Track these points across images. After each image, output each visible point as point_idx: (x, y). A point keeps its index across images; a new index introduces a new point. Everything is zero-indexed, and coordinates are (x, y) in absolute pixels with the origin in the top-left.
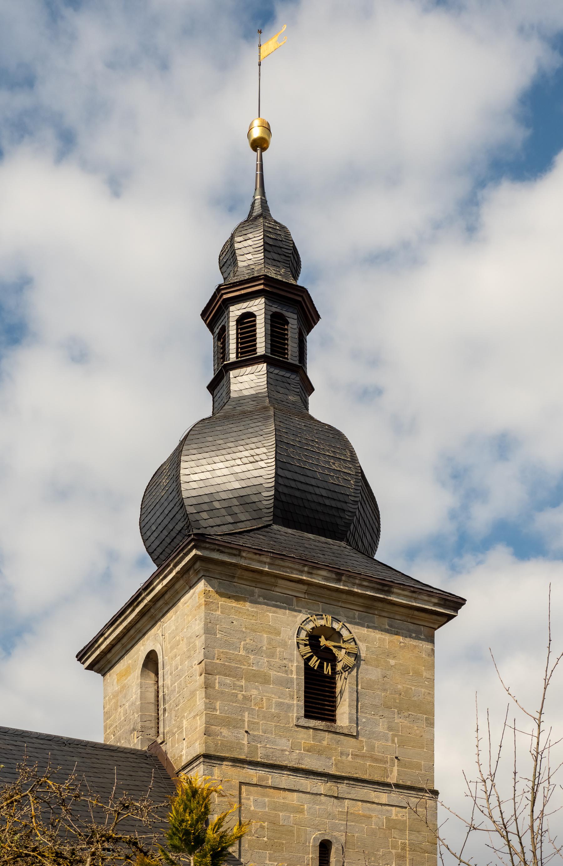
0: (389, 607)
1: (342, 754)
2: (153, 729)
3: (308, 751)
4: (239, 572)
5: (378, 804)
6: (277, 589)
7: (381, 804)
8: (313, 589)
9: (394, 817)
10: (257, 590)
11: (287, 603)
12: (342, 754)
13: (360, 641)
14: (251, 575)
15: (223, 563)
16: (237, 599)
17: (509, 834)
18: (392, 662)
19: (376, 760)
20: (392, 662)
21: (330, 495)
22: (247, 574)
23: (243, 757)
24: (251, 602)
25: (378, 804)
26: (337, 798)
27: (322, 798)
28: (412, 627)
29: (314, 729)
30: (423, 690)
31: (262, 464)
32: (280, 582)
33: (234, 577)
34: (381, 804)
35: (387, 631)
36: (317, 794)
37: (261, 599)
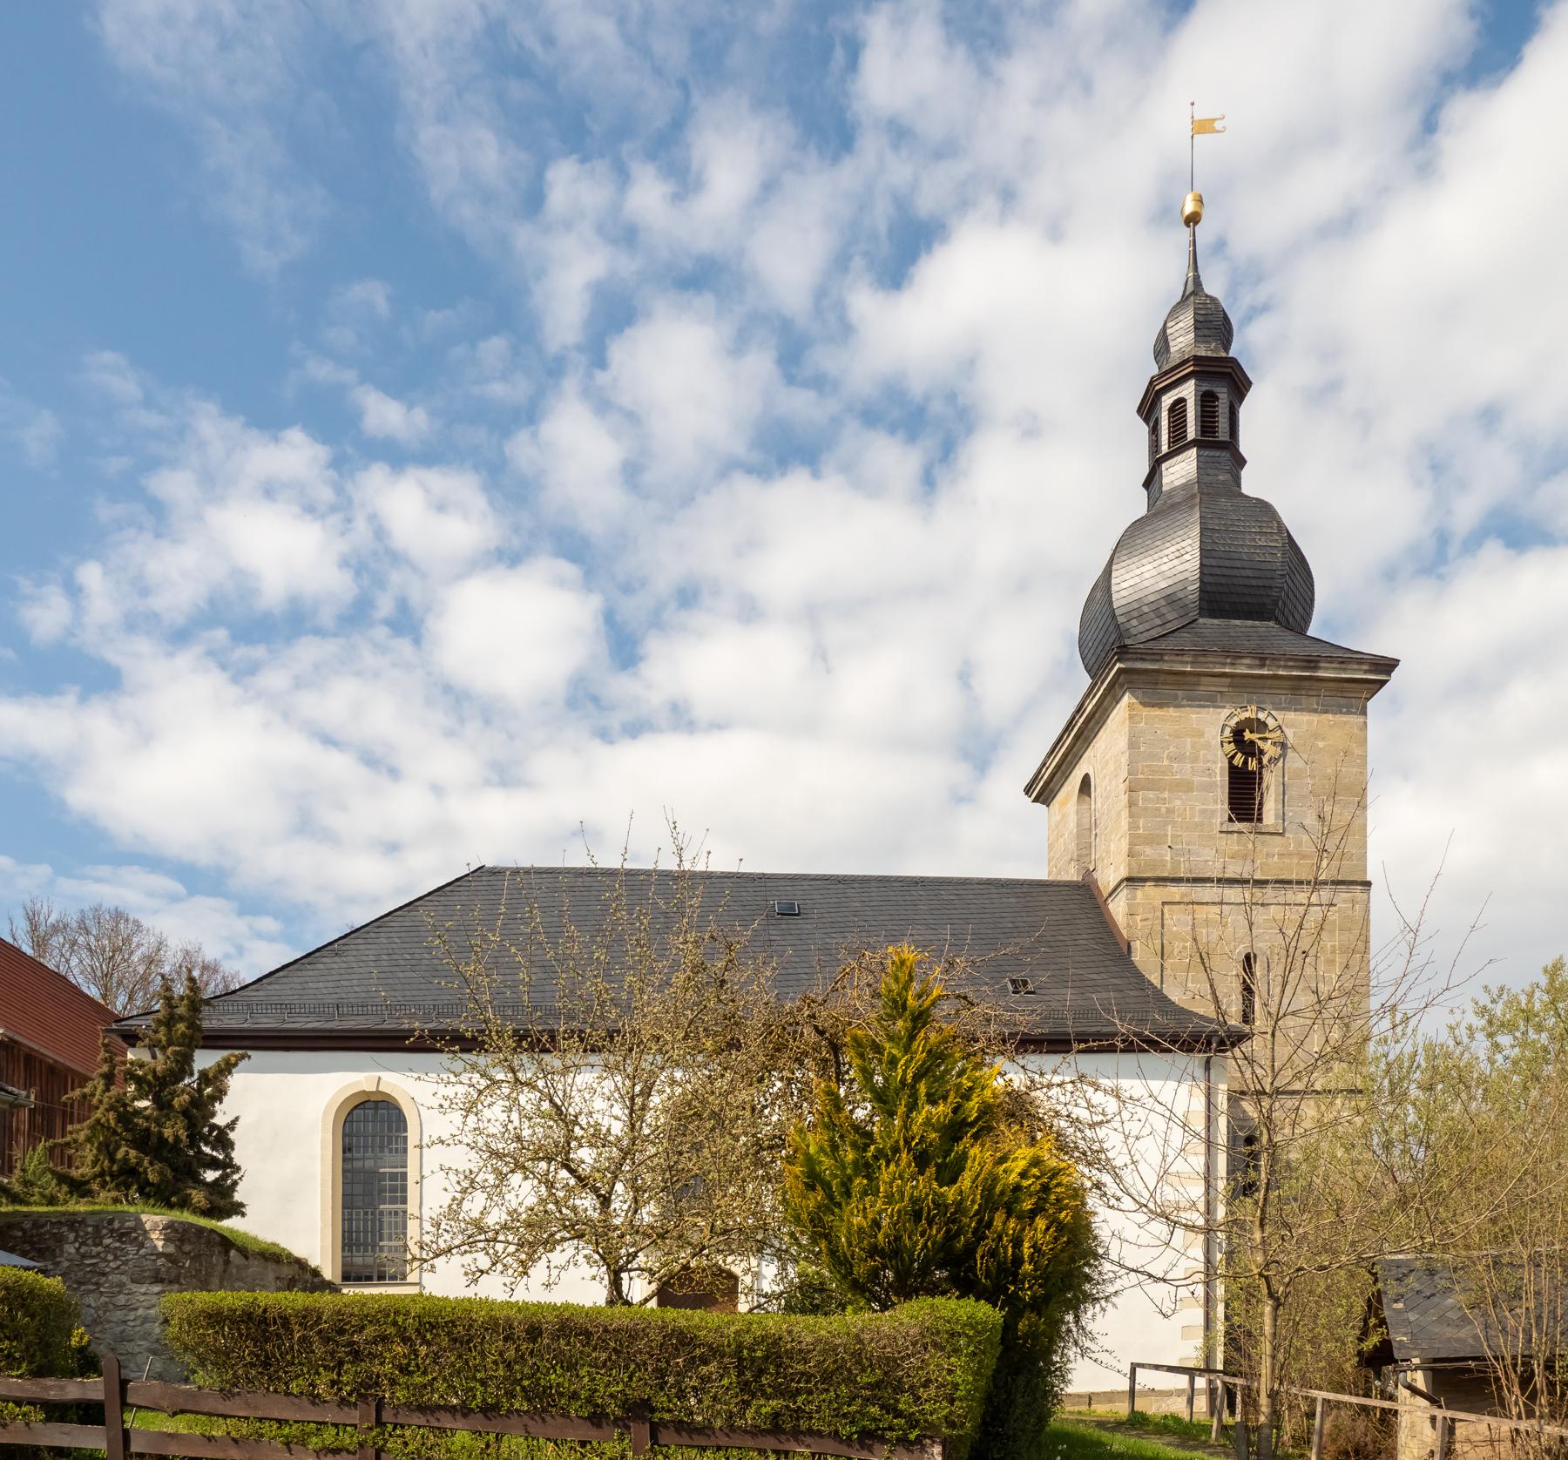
0: (1316, 684)
8: (1236, 681)
11: (1211, 701)
18: (1321, 744)
20: (1321, 744)
21: (1256, 574)
23: (1166, 875)
28: (1342, 701)
31: (1187, 557)
32: (1204, 679)
35: (1315, 711)
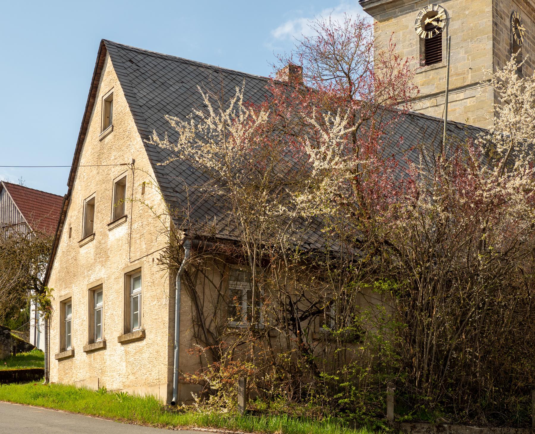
1: (440, 79)
2: (443, 106)
3: (423, 85)
4: (385, 6)
5: (459, 100)
6: (406, 4)
7: (461, 100)
9: (469, 105)
10: (397, 10)
12: (440, 79)
13: (449, 9)
14: (391, 5)
15: (377, 6)
16: (388, 20)
17: (450, 88)
18: (467, 12)
19: (459, 75)
20: (467, 12)
22: (389, 6)
24: (395, 18)
25: (459, 100)
26: (437, 106)
27: (430, 109)
29: (425, 72)
30: (485, 20)
33: (385, 10)
34: (461, 100)
36: (426, 108)
37: (399, 14)
